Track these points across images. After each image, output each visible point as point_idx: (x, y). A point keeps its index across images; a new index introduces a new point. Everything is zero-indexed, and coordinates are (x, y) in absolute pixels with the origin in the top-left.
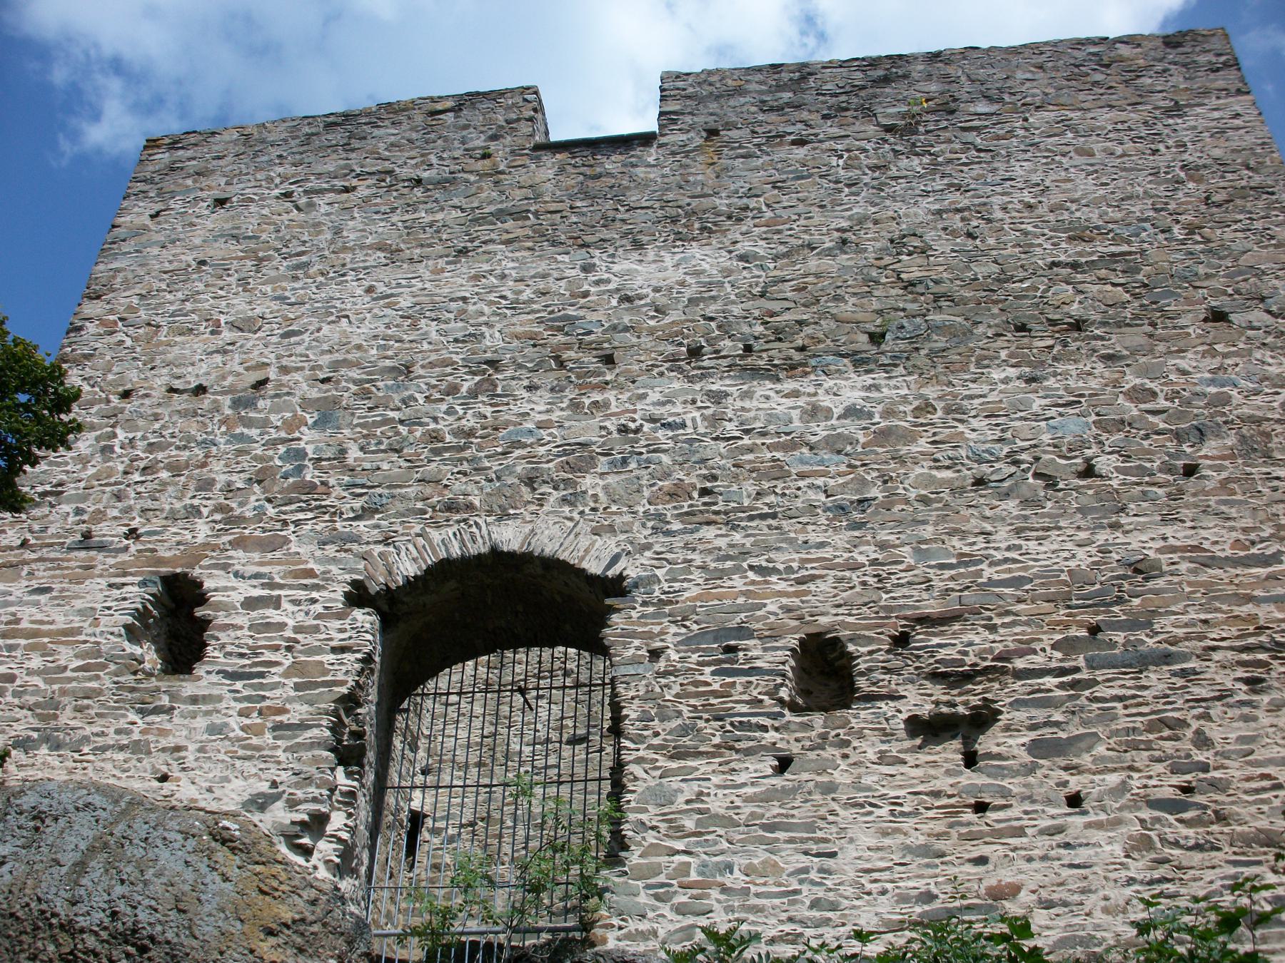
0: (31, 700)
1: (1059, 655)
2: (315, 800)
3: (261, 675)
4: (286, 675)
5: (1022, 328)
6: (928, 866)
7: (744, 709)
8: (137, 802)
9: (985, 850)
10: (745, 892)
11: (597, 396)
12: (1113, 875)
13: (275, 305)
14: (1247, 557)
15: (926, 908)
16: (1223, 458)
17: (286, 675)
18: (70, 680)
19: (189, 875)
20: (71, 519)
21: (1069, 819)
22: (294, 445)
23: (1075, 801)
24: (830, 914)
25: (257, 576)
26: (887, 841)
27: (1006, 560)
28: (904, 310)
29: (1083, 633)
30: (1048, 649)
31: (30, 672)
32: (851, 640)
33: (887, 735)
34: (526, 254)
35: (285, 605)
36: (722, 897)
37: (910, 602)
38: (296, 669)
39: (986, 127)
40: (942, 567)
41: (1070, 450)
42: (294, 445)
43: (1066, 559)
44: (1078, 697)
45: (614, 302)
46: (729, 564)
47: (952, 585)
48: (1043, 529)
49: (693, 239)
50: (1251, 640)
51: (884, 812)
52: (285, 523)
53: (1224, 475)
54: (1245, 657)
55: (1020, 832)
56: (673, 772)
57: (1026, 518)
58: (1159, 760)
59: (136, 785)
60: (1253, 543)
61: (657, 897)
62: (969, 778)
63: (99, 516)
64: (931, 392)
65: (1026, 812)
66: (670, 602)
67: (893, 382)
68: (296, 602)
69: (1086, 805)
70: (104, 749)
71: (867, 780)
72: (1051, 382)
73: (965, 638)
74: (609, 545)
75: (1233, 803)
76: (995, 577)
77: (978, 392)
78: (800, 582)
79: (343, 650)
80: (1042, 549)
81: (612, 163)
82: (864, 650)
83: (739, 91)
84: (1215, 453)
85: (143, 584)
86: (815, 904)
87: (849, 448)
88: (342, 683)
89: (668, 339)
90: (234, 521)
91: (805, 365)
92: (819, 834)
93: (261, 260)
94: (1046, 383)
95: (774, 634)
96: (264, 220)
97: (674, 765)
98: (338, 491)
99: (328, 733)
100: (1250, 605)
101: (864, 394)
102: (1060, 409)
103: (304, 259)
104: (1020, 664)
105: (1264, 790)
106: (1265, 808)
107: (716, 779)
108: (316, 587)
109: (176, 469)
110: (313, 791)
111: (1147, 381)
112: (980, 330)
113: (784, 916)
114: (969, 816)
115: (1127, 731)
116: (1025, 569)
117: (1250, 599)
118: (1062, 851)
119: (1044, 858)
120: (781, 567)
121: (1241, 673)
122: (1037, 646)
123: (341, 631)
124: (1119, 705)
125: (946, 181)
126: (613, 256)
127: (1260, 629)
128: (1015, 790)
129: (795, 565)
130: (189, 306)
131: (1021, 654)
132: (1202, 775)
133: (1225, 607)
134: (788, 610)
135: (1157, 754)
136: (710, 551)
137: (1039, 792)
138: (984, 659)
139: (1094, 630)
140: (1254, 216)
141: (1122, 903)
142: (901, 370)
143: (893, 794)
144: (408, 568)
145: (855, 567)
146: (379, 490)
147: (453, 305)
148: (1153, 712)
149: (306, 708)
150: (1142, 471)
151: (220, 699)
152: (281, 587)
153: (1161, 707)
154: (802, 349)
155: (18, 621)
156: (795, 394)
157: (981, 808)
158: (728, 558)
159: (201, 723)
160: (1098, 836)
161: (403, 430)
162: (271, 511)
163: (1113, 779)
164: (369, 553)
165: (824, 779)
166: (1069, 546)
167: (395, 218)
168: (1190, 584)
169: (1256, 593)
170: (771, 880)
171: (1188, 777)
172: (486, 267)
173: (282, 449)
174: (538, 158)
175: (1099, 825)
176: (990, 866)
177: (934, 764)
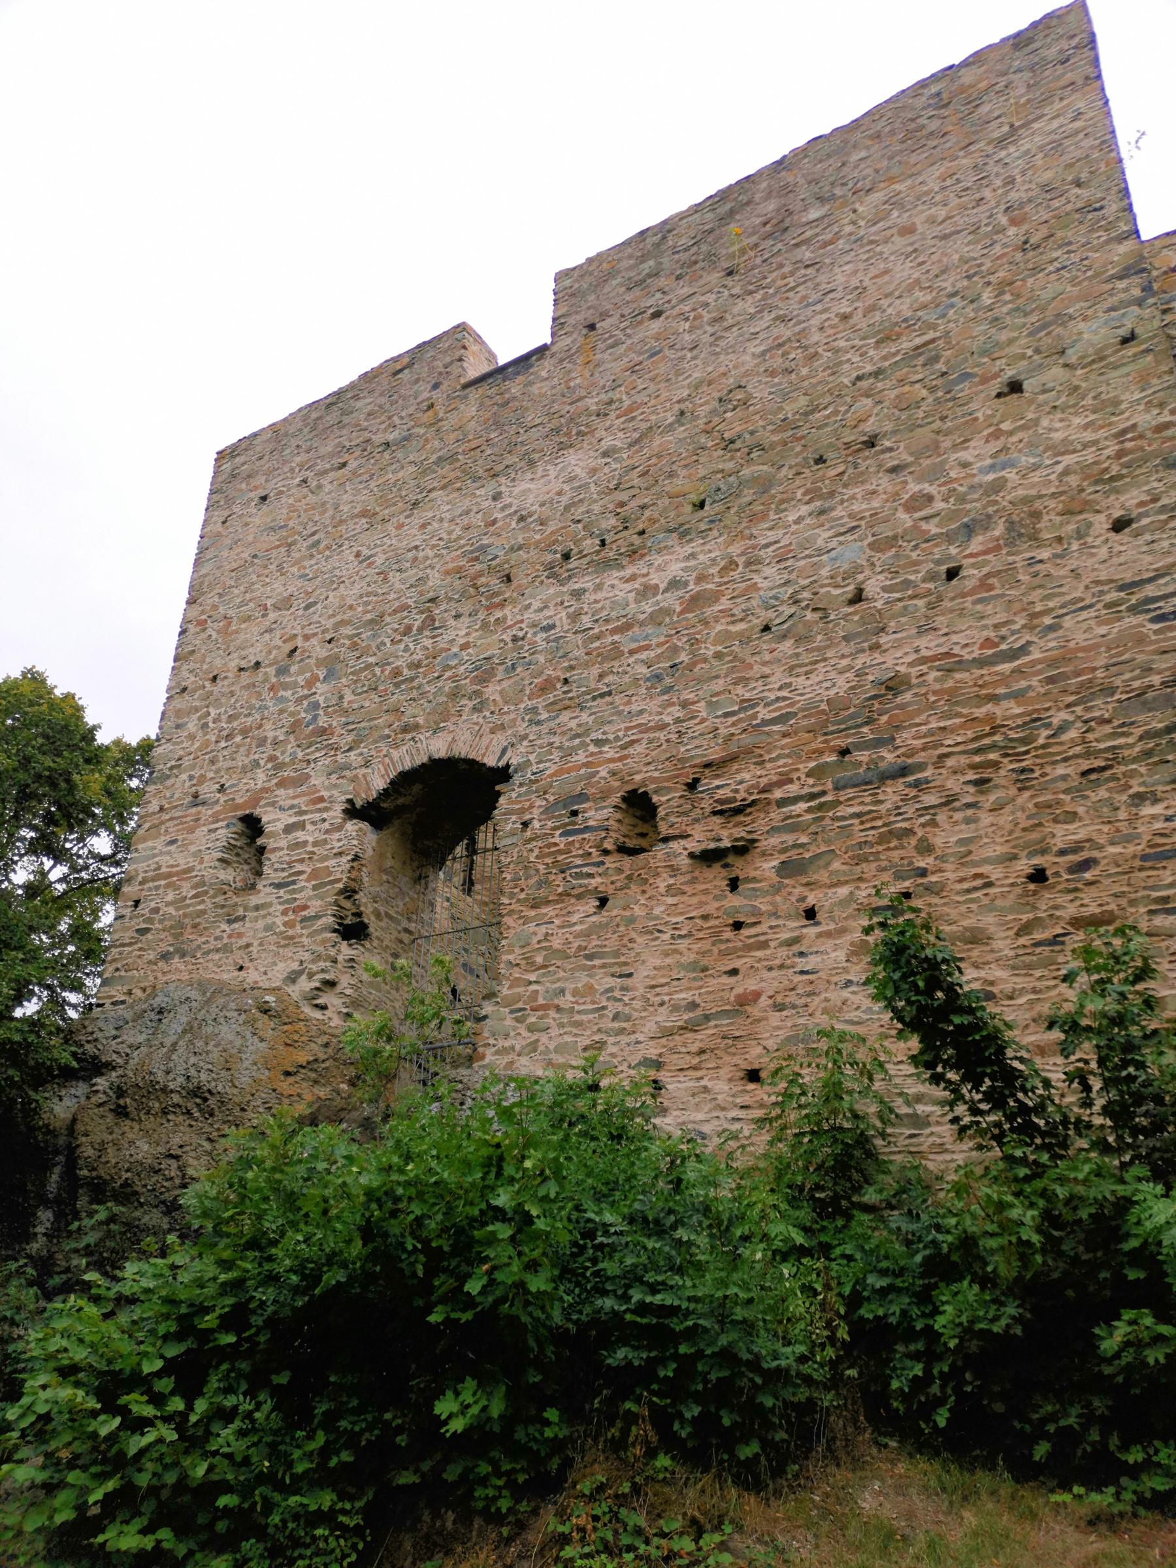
0: (168, 923)
1: (811, 781)
2: (323, 971)
3: (294, 882)
4: (308, 880)
5: (820, 460)
6: (694, 979)
7: (579, 862)
8: (220, 989)
9: (737, 964)
10: (571, 1010)
11: (499, 614)
12: (835, 979)
13: (299, 583)
14: (994, 655)
15: (691, 1015)
16: (985, 553)
17: (308, 880)
18: (189, 906)
19: (238, 1042)
20: (187, 784)
21: (805, 931)
22: (312, 699)
23: (810, 914)
24: (624, 1025)
25: (292, 807)
26: (668, 961)
27: (778, 699)
28: (722, 471)
29: (832, 758)
30: (803, 777)
31: (168, 904)
32: (656, 792)
33: (674, 870)
34: (456, 495)
35: (309, 827)
36: (557, 1016)
37: (699, 752)
38: (315, 874)
39: (817, 235)
40: (727, 715)
41: (844, 579)
42: (312, 699)
43: (827, 689)
44: (822, 818)
45: (514, 524)
46: (577, 741)
47: (733, 730)
48: (811, 663)
49: (571, 446)
50: (986, 741)
51: (666, 937)
52: (309, 762)
53: (985, 570)
54: (977, 759)
55: (764, 945)
56: (532, 919)
57: (797, 655)
58: (884, 869)
59: (225, 976)
60: (1003, 638)
61: (517, 1020)
62: (734, 901)
63: (202, 779)
64: (735, 550)
65: (771, 927)
66: (537, 781)
67: (707, 547)
68: (314, 823)
69: (819, 917)
70: (207, 953)
71: (657, 911)
72: (839, 512)
73: (738, 777)
74: (500, 740)
75: (944, 904)
76: (768, 717)
77: (772, 539)
78: (623, 748)
79: (340, 854)
80: (809, 682)
81: (515, 388)
82: (664, 799)
83: (611, 275)
84: (980, 548)
85: (228, 826)
86: (616, 1017)
87: (667, 620)
88: (339, 880)
89: (548, 548)
90: (279, 767)
91: (644, 547)
92: (623, 959)
93: (290, 545)
94: (833, 514)
95: (604, 795)
96: (292, 509)
97: (533, 913)
98: (339, 731)
99: (332, 919)
100: (989, 706)
101: (683, 565)
102: (841, 538)
103: (316, 537)
104: (778, 794)
105: (976, 889)
106: (974, 906)
107: (557, 922)
108: (326, 809)
109: (245, 732)
110: (322, 964)
111: (926, 485)
112: (784, 471)
113: (595, 1028)
114: (728, 934)
115: (860, 845)
116: (791, 705)
117: (994, 698)
118: (798, 960)
119: (781, 967)
120: (611, 737)
121: (971, 776)
122: (795, 776)
123: (339, 840)
124: (856, 821)
125: (773, 315)
126: (514, 480)
127: (995, 730)
128: (763, 908)
129: (620, 734)
130: (248, 596)
131: (780, 784)
132: (920, 881)
133: (965, 711)
134: (613, 773)
135: (884, 864)
136: (563, 733)
137: (784, 907)
138: (751, 794)
139: (844, 752)
140: (1073, 248)
141: (839, 1003)
142: (715, 533)
143: (674, 920)
144: (379, 783)
145: (662, 727)
146: (363, 725)
147: (410, 555)
148: (885, 825)
149: (319, 903)
150: (907, 583)
151: (270, 904)
152: (305, 813)
153: (892, 819)
154: (642, 533)
155: (159, 868)
156: (633, 578)
157: (738, 926)
158: (577, 736)
159: (261, 924)
160: (829, 944)
161: (377, 670)
162: (300, 755)
163: (843, 891)
164: (356, 776)
165: (628, 913)
166: (832, 675)
167: (373, 484)
168: (935, 693)
169: (998, 691)
170: (588, 999)
171: (907, 884)
172: (430, 514)
173: (305, 703)
174: (466, 397)
175: (828, 934)
176: (740, 977)
177: (706, 892)
